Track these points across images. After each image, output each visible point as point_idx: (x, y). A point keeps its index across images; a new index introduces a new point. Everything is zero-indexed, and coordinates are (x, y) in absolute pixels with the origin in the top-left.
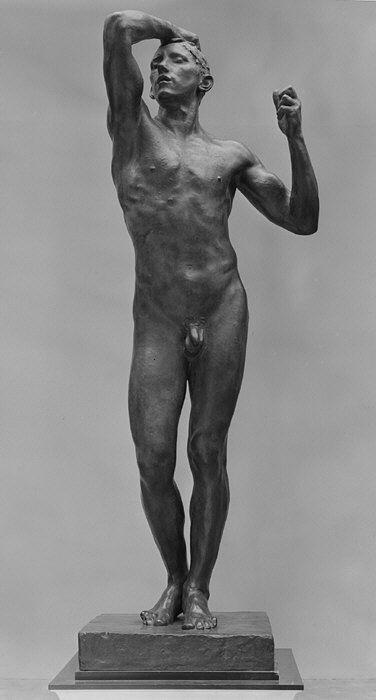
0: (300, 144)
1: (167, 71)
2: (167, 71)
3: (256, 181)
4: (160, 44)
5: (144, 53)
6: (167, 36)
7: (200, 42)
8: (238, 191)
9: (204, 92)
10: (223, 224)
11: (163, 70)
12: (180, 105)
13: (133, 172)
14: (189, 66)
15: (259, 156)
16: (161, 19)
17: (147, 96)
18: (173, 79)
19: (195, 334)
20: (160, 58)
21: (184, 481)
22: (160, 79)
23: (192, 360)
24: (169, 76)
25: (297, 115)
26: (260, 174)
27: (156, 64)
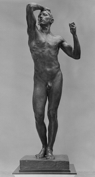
0: (76, 36)
1: (42, 18)
2: (42, 18)
4: (40, 11)
5: (36, 13)
6: (42, 9)
7: (51, 11)
8: (60, 48)
9: (52, 23)
10: (56, 57)
11: (41, 18)
12: (45, 27)
13: (34, 43)
14: (48, 17)
15: (65, 40)
16: (41, 5)
17: (37, 24)
18: (44, 20)
19: (49, 84)
20: (40, 15)
21: (47, 122)
22: (41, 20)
24: (43, 19)
25: (75, 29)
26: (66, 44)
27: (39, 16)
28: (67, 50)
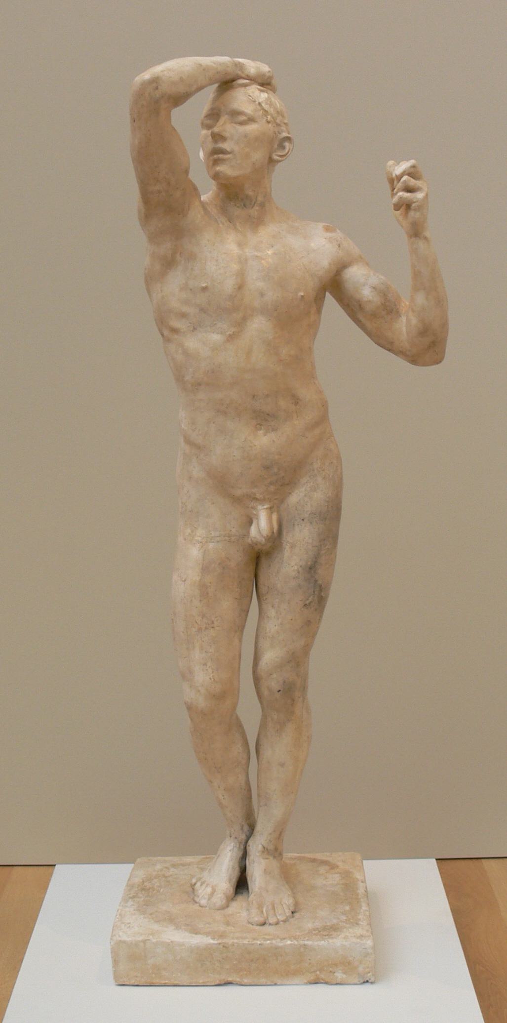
1: (223, 139)
2: (223, 139)
5: (188, 121)
8: (328, 294)
11: (218, 137)
20: (214, 115)
23: (416, 232)
24: (226, 146)
28: (372, 319)
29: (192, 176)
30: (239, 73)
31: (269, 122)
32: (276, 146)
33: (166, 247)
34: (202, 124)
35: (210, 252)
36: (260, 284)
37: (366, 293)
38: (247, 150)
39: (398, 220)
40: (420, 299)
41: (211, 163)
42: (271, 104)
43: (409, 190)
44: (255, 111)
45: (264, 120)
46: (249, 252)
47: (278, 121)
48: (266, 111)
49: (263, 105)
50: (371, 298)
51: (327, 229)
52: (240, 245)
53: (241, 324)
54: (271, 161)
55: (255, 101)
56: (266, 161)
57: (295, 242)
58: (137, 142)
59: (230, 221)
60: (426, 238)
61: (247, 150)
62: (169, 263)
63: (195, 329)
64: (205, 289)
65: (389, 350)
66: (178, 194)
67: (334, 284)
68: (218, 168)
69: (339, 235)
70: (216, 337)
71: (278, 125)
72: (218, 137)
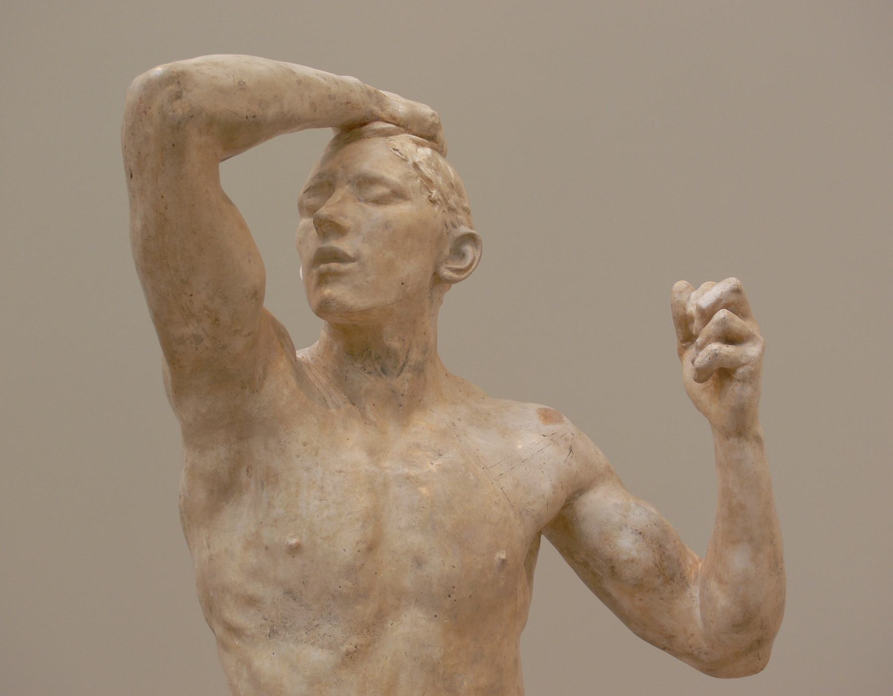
1: (339, 230)
2: (339, 230)
3: (707, 359)
5: (263, 187)
7: (442, 135)
8: (543, 537)
11: (328, 228)
16: (110, 218)
20: (324, 185)
22: (324, 256)
23: (739, 426)
24: (345, 245)
28: (636, 593)
29: (270, 304)
30: (376, 109)
31: (433, 202)
32: (447, 252)
33: (217, 456)
34: (301, 207)
35: (308, 469)
36: (416, 540)
37: (627, 545)
38: (389, 254)
39: (696, 402)
40: (739, 560)
41: (314, 281)
42: (437, 169)
43: (730, 338)
44: (407, 177)
45: (425, 197)
46: (392, 466)
47: (451, 202)
48: (429, 181)
49: (422, 168)
50: (634, 554)
51: (547, 417)
52: (372, 452)
53: (374, 626)
54: (438, 281)
55: (405, 160)
56: (428, 280)
57: (483, 442)
58: (139, 224)
59: (353, 400)
60: (758, 439)
61: (389, 254)
62: (223, 489)
63: (273, 633)
64: (295, 550)
65: (664, 649)
66: (239, 344)
67: (563, 526)
68: (327, 291)
69: (567, 427)
70: (317, 657)
71: (451, 209)
72: (328, 228)
